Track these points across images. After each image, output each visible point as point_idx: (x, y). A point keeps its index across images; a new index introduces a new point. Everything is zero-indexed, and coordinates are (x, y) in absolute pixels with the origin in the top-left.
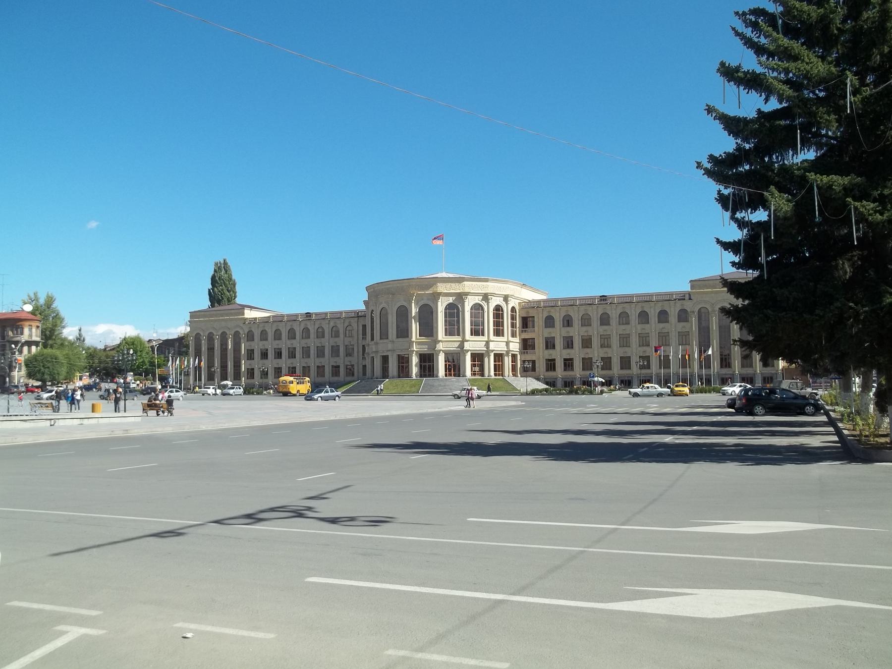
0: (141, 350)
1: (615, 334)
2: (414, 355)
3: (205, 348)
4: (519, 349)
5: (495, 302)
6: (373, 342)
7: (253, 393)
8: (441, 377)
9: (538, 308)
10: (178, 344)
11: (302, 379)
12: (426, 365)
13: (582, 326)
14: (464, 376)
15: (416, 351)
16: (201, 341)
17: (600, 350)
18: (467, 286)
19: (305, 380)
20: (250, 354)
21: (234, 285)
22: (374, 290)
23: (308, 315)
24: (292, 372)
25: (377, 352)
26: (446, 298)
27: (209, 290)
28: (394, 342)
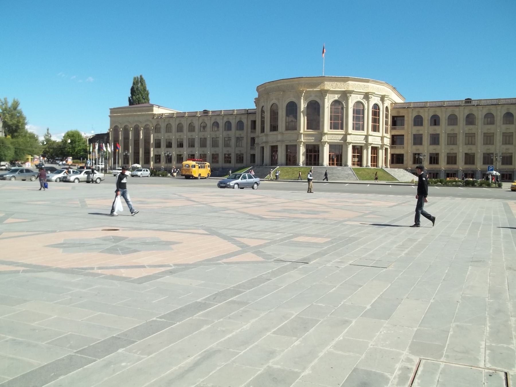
0: (79, 141)
1: (479, 133)
2: (301, 145)
3: (121, 138)
4: (390, 144)
5: (374, 100)
6: (263, 134)
7: (158, 176)
8: (325, 166)
9: (408, 109)
10: (106, 138)
11: (203, 164)
12: (312, 155)
13: (448, 125)
14: (346, 165)
15: (303, 142)
16: (119, 132)
17: (465, 146)
18: (351, 85)
19: (206, 165)
20: (158, 145)
21: (148, 94)
22: (265, 88)
23: (206, 112)
24: (192, 157)
25: (266, 142)
26: (332, 95)
27: (129, 98)
28: (283, 133)
